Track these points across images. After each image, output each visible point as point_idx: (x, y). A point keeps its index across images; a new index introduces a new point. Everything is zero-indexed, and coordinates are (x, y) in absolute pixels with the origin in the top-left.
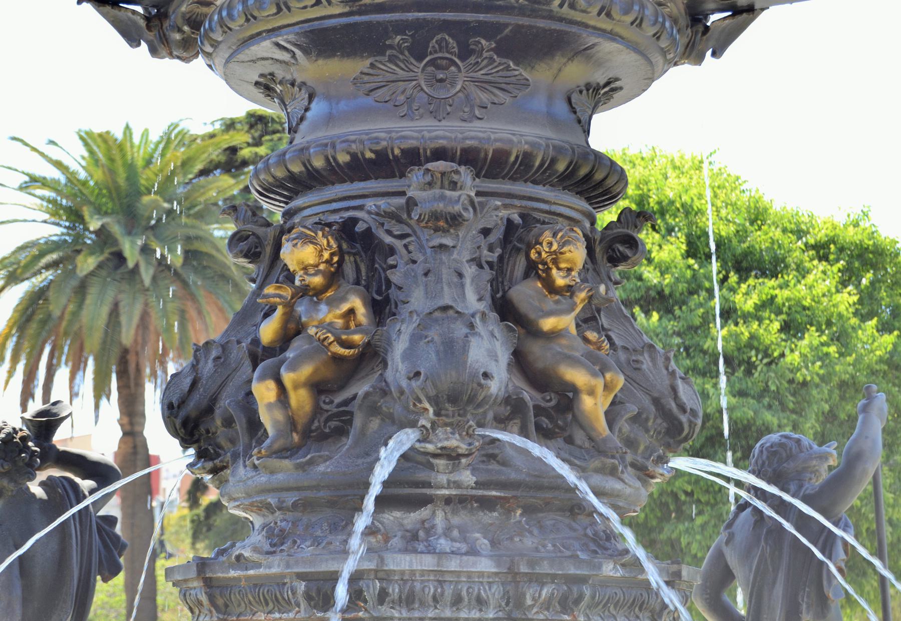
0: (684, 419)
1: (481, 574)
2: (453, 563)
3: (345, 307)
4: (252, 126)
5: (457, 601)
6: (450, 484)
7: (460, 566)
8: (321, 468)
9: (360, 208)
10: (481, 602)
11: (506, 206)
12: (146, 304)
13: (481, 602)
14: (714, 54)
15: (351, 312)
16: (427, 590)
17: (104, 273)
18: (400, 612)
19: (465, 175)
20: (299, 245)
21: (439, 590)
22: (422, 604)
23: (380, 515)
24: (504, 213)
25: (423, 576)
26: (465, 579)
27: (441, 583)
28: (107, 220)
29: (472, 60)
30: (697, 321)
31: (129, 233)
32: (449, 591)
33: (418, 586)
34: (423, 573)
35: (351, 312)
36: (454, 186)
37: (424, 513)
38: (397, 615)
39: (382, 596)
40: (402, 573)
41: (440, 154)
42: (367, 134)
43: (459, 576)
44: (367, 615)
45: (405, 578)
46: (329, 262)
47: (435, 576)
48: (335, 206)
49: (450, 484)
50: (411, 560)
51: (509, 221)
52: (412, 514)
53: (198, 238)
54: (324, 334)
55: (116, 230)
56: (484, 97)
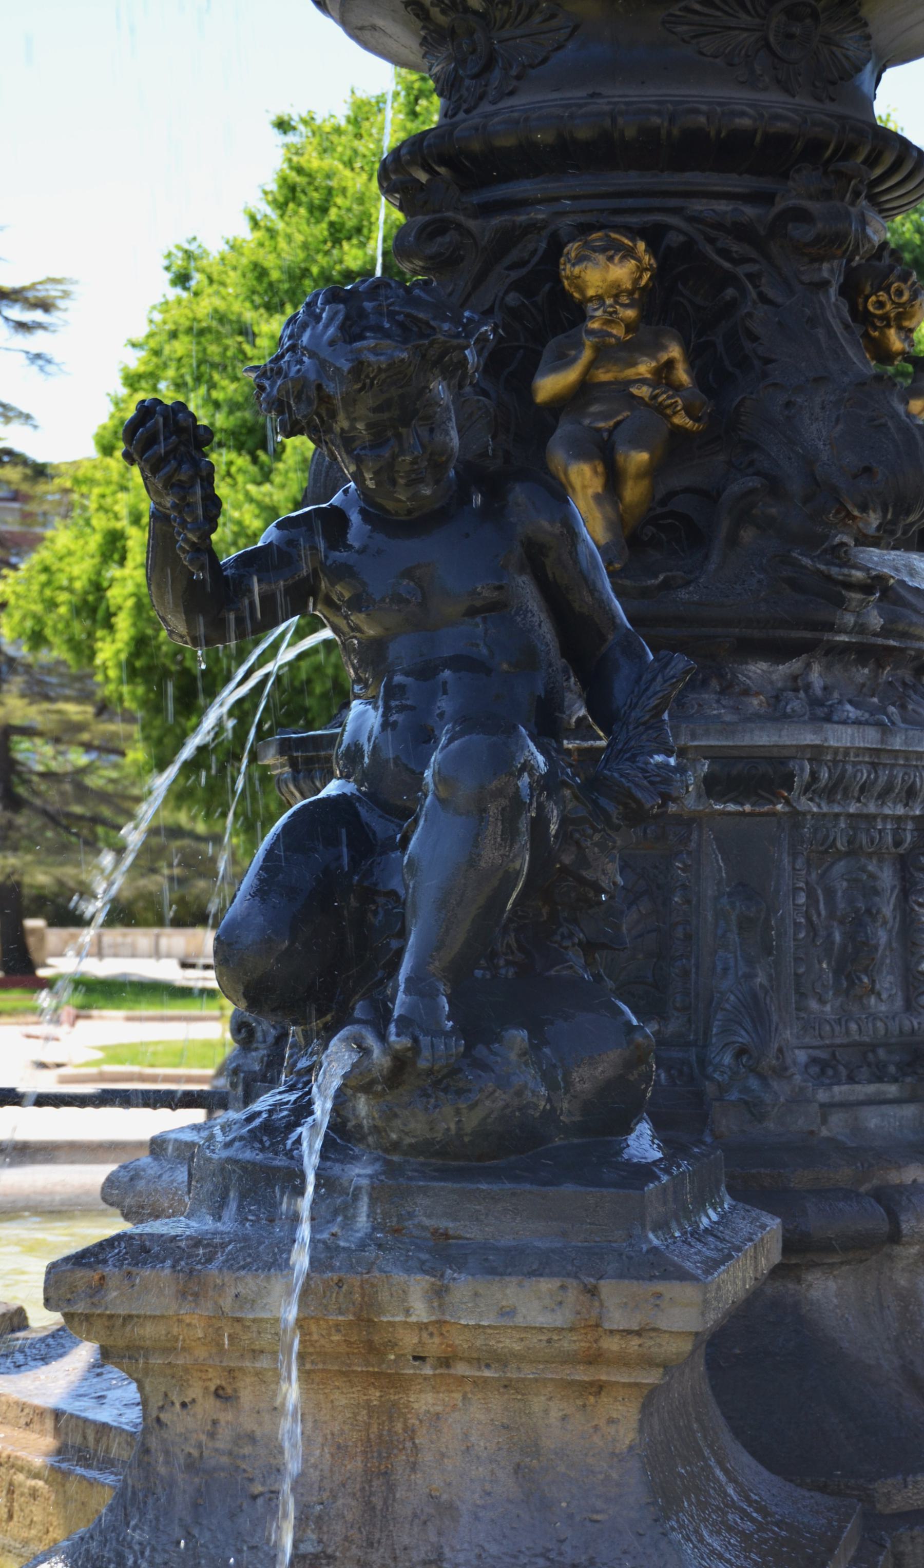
2: (898, 739)
7: (906, 743)
8: (683, 595)
16: (859, 775)
18: (819, 806)
20: (617, 259)
21: (872, 776)
23: (744, 667)
25: (857, 755)
26: (902, 762)
33: (849, 768)
37: (795, 665)
38: (815, 809)
40: (836, 750)
42: (720, 104)
43: (896, 758)
44: (787, 809)
47: (871, 757)
48: (630, 202)
50: (853, 734)
52: (781, 667)
54: (669, 398)
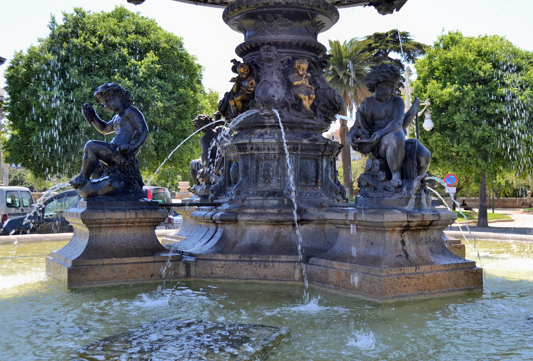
0: (337, 106)
1: (273, 143)
3: (250, 82)
4: (376, 38)
5: (269, 149)
6: (269, 123)
9: (254, 58)
10: (274, 149)
11: (288, 55)
12: (345, 90)
13: (274, 149)
14: (396, 11)
15: (252, 83)
17: (334, 81)
19: (273, 48)
22: (261, 150)
24: (287, 57)
27: (265, 145)
28: (334, 67)
29: (278, 20)
30: (494, 87)
31: (341, 70)
32: (266, 147)
34: (260, 143)
35: (252, 83)
36: (270, 51)
37: (265, 129)
39: (252, 149)
41: (269, 44)
45: (257, 144)
46: (247, 71)
49: (269, 123)
51: (289, 59)
53: (360, 70)
55: (337, 69)
56: (281, 28)
